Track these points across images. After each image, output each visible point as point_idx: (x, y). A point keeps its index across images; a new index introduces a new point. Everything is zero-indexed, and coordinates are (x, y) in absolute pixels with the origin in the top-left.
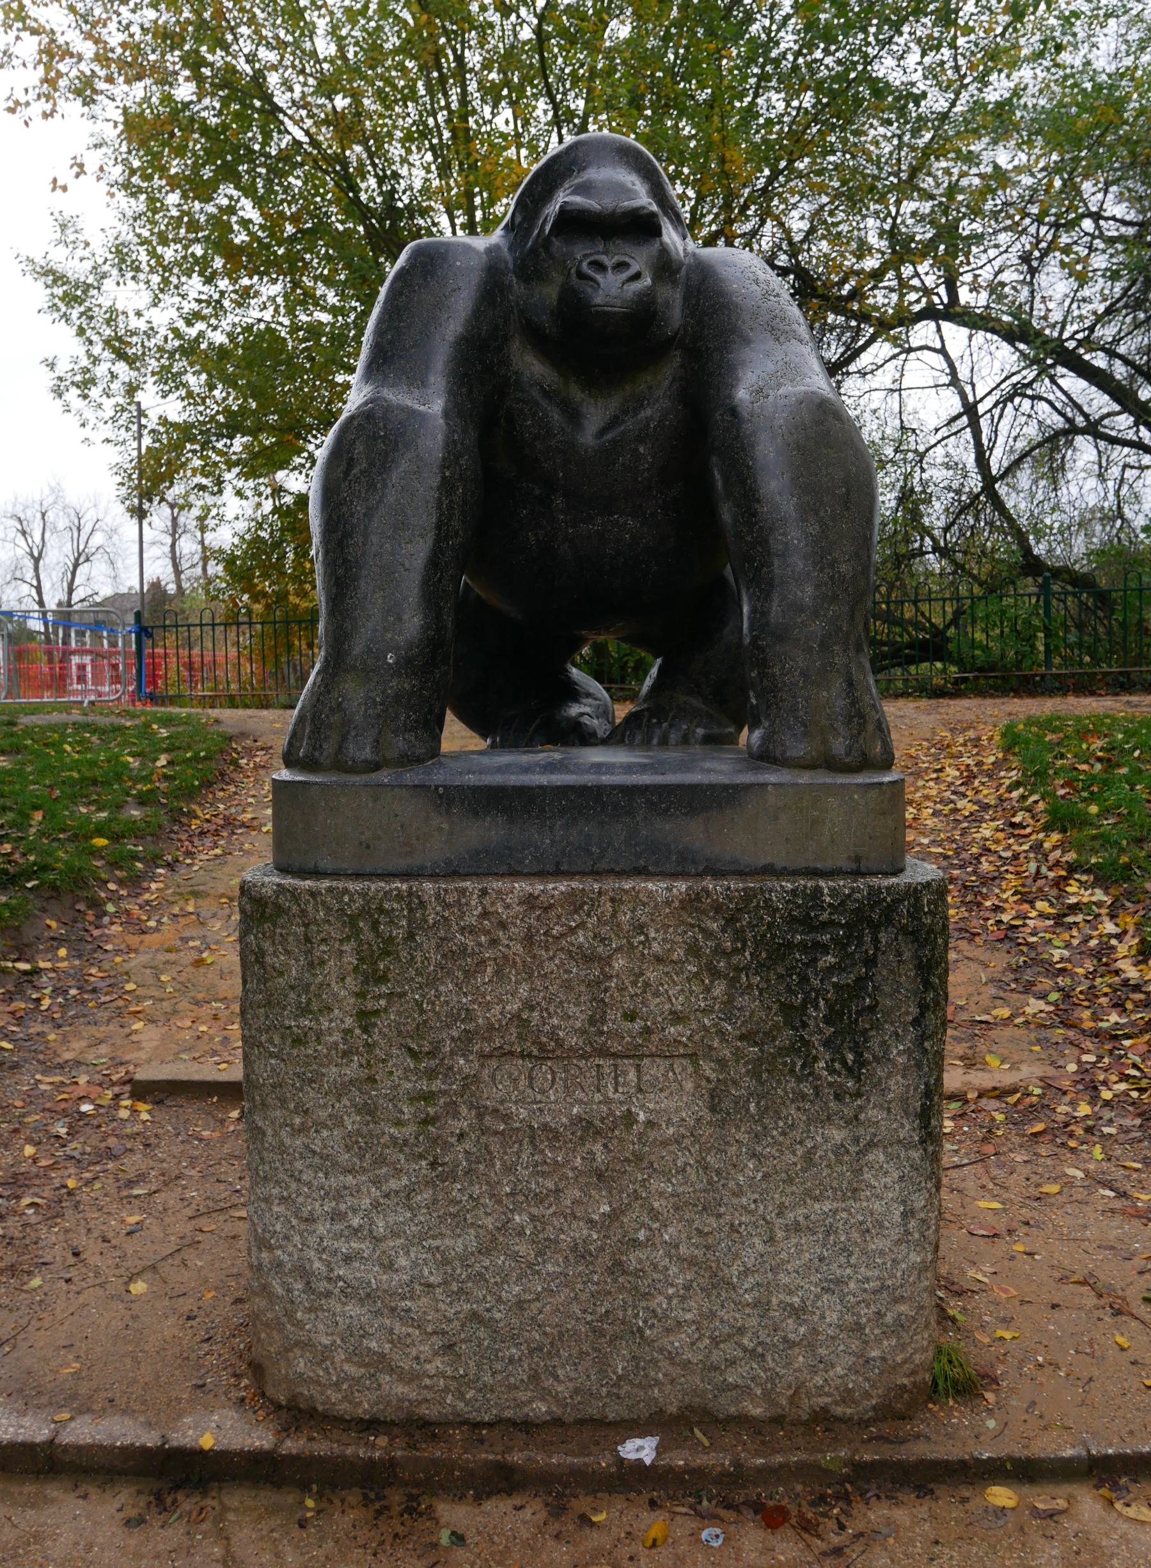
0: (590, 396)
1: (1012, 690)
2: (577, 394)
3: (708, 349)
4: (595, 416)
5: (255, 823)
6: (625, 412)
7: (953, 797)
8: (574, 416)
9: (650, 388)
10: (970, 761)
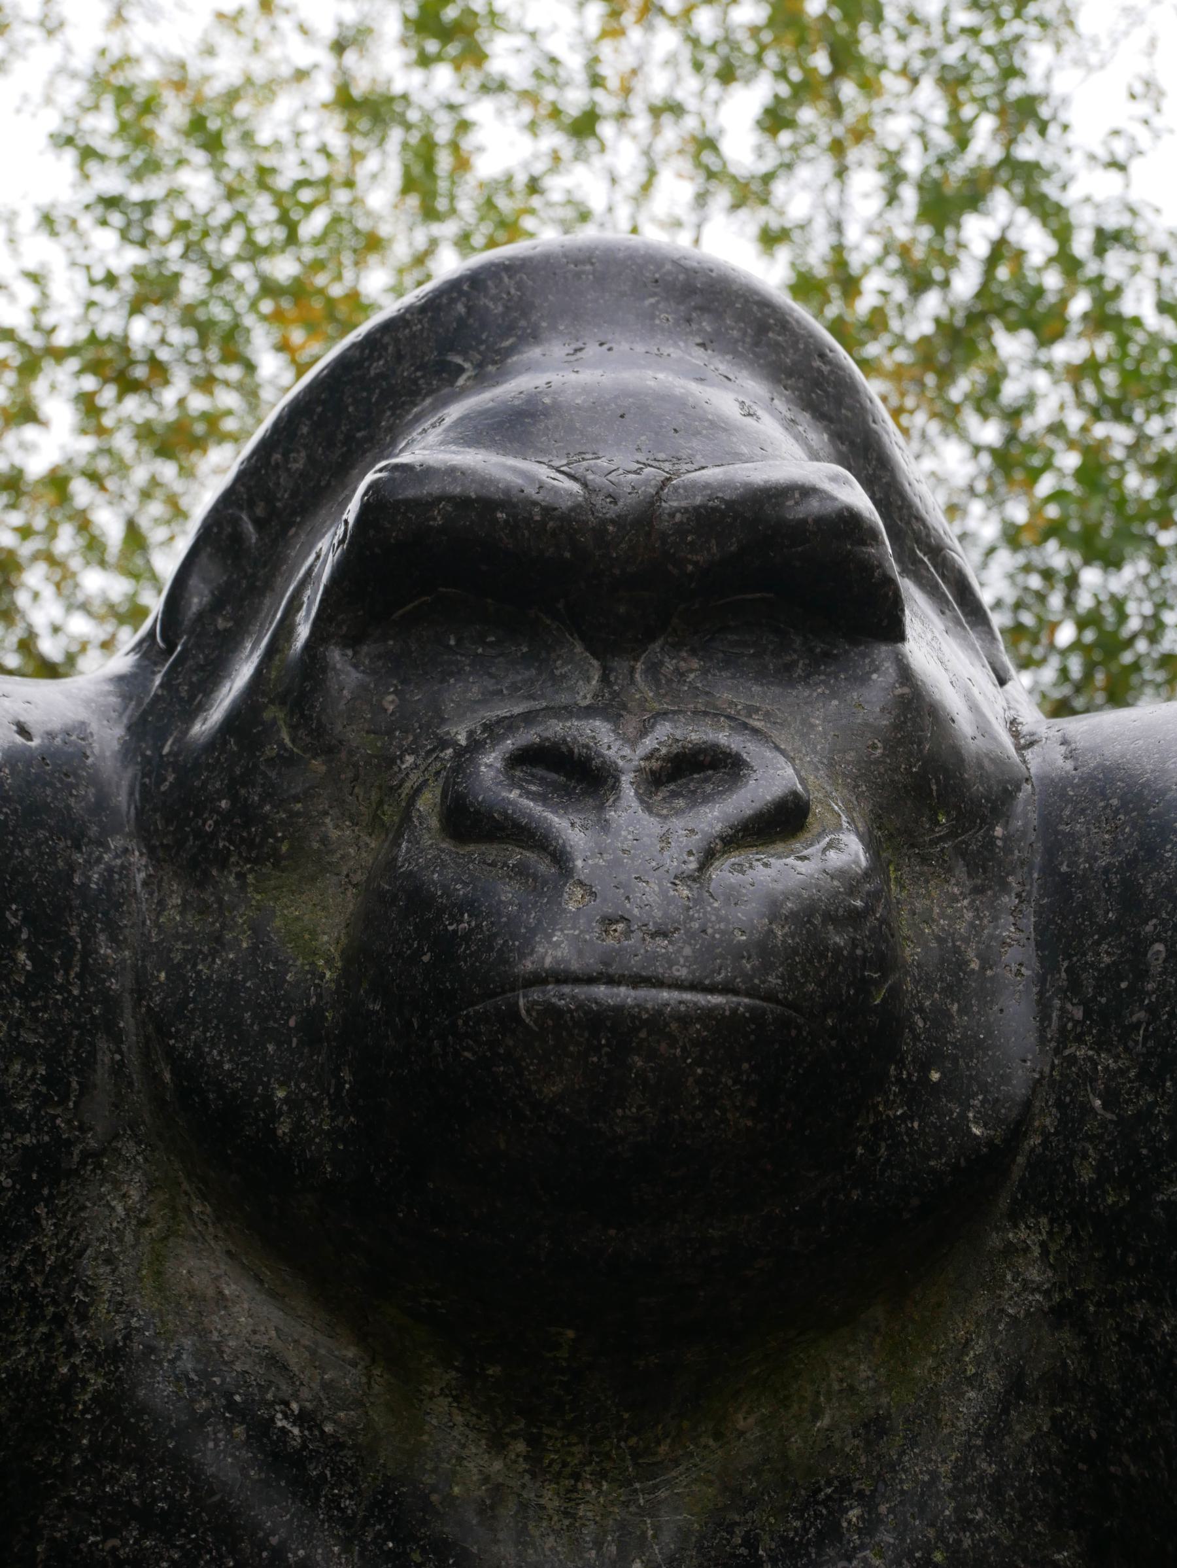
9: (875, 1428)
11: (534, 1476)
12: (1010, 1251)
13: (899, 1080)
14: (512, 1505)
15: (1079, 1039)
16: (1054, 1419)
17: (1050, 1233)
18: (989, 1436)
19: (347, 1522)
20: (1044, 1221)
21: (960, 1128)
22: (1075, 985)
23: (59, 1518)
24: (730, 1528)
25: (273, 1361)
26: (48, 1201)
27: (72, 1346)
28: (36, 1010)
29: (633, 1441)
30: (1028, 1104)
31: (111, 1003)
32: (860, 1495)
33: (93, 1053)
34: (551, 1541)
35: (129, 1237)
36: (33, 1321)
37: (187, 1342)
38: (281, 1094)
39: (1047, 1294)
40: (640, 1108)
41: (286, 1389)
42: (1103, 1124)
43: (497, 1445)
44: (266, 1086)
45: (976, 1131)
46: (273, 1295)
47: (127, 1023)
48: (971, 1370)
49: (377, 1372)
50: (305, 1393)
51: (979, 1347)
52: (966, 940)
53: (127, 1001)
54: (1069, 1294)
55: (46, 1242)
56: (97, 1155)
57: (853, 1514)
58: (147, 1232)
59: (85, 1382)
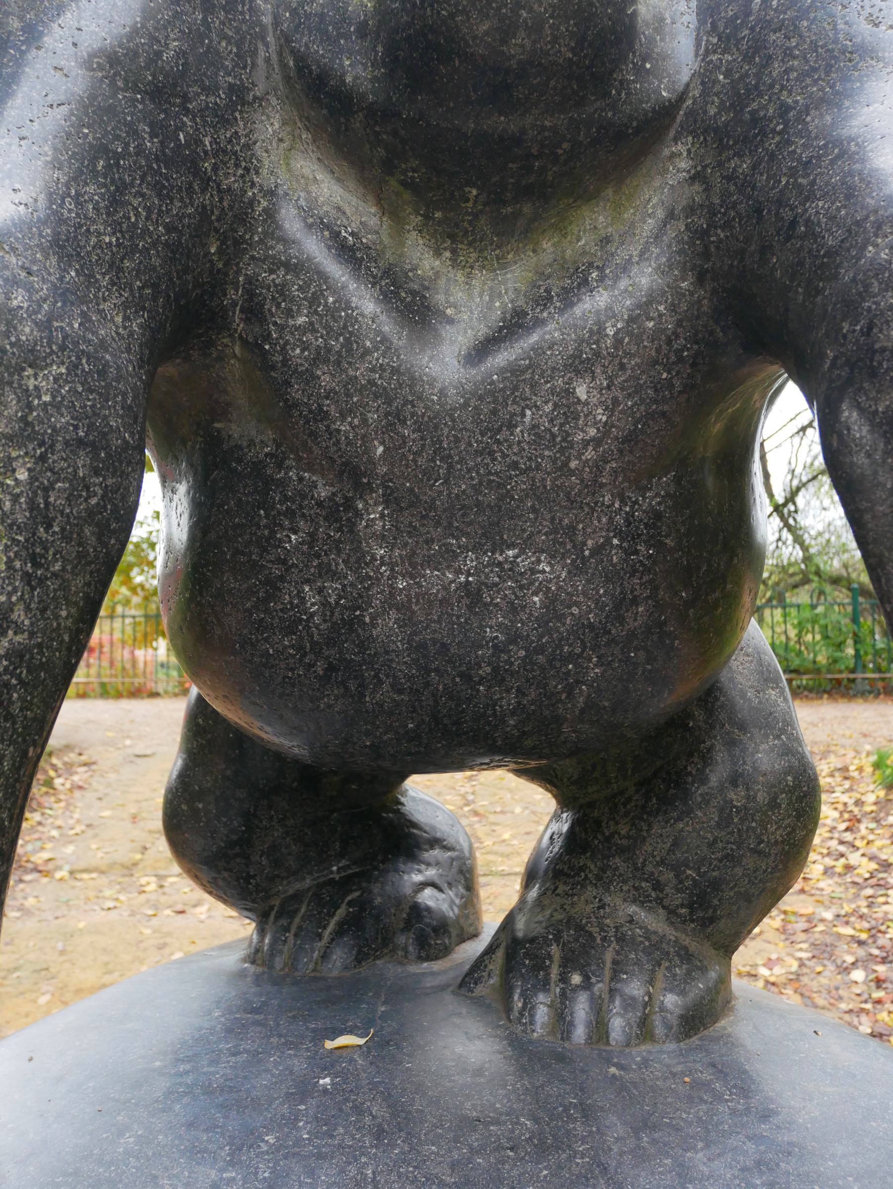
0: (454, 262)
1: (825, 691)
2: (422, 258)
3: (784, 109)
4: (471, 301)
5: (51, 866)
6: (544, 301)
7: (842, 848)
8: (416, 310)
9: (606, 241)
10: (845, 798)
11: (453, 267)
12: (673, 156)
13: (633, 62)
14: (444, 280)
15: (715, 52)
16: (686, 225)
17: (693, 144)
18: (656, 237)
19: (374, 277)
20: (690, 138)
21: (657, 92)
22: (714, 25)
23: (249, 264)
24: (539, 287)
25: (339, 209)
26: (241, 112)
27: (253, 185)
28: (230, 20)
29: (497, 252)
30: (688, 85)
31: (263, 28)
32: (598, 267)
33: (256, 49)
34: (460, 294)
35: (274, 144)
36: (237, 166)
37: (302, 194)
38: (348, 63)
39: (689, 172)
40: (523, 39)
41: (346, 222)
42: (723, 86)
43: (438, 253)
44: (341, 59)
45: (664, 94)
46: (339, 180)
47: (270, 39)
48: (650, 211)
49: (385, 219)
50: (353, 225)
51: (655, 200)
52: (666, 10)
53: (270, 29)
54: (699, 168)
55: (241, 132)
56: (261, 99)
57: (594, 275)
58: (282, 145)
59: (259, 202)
